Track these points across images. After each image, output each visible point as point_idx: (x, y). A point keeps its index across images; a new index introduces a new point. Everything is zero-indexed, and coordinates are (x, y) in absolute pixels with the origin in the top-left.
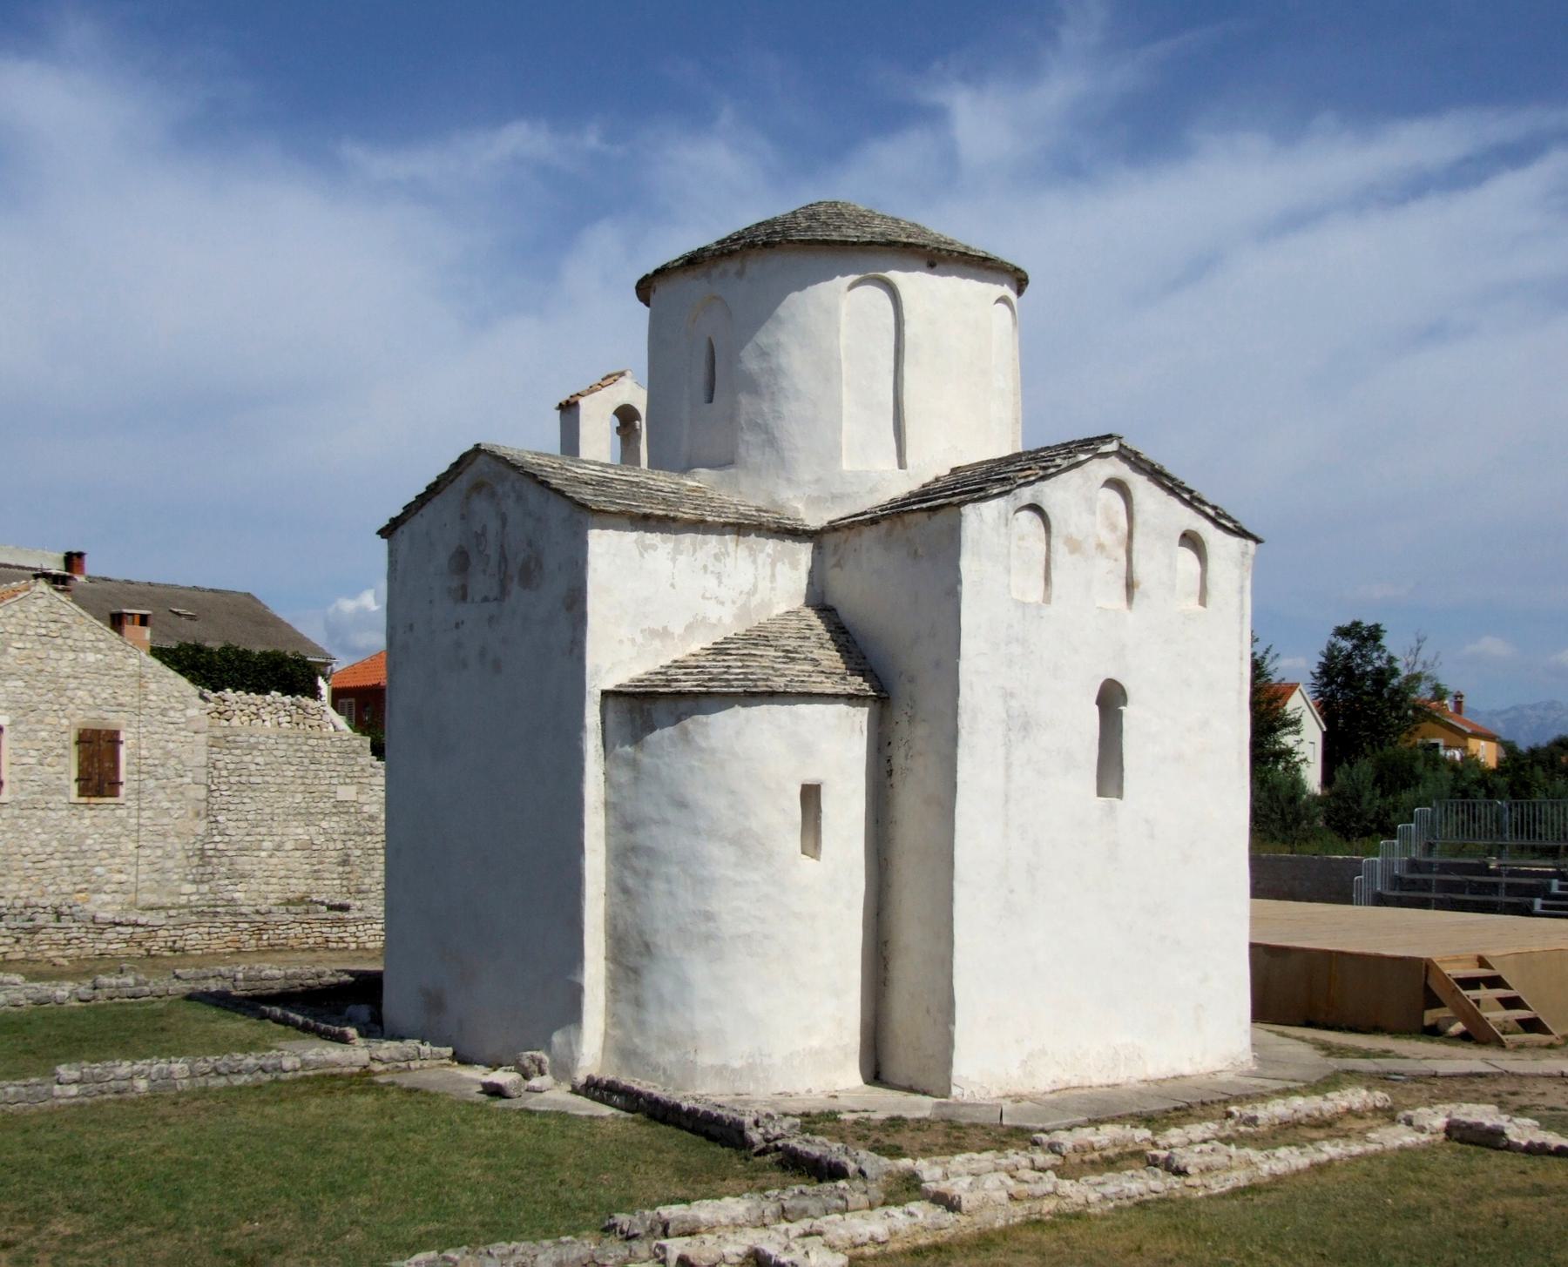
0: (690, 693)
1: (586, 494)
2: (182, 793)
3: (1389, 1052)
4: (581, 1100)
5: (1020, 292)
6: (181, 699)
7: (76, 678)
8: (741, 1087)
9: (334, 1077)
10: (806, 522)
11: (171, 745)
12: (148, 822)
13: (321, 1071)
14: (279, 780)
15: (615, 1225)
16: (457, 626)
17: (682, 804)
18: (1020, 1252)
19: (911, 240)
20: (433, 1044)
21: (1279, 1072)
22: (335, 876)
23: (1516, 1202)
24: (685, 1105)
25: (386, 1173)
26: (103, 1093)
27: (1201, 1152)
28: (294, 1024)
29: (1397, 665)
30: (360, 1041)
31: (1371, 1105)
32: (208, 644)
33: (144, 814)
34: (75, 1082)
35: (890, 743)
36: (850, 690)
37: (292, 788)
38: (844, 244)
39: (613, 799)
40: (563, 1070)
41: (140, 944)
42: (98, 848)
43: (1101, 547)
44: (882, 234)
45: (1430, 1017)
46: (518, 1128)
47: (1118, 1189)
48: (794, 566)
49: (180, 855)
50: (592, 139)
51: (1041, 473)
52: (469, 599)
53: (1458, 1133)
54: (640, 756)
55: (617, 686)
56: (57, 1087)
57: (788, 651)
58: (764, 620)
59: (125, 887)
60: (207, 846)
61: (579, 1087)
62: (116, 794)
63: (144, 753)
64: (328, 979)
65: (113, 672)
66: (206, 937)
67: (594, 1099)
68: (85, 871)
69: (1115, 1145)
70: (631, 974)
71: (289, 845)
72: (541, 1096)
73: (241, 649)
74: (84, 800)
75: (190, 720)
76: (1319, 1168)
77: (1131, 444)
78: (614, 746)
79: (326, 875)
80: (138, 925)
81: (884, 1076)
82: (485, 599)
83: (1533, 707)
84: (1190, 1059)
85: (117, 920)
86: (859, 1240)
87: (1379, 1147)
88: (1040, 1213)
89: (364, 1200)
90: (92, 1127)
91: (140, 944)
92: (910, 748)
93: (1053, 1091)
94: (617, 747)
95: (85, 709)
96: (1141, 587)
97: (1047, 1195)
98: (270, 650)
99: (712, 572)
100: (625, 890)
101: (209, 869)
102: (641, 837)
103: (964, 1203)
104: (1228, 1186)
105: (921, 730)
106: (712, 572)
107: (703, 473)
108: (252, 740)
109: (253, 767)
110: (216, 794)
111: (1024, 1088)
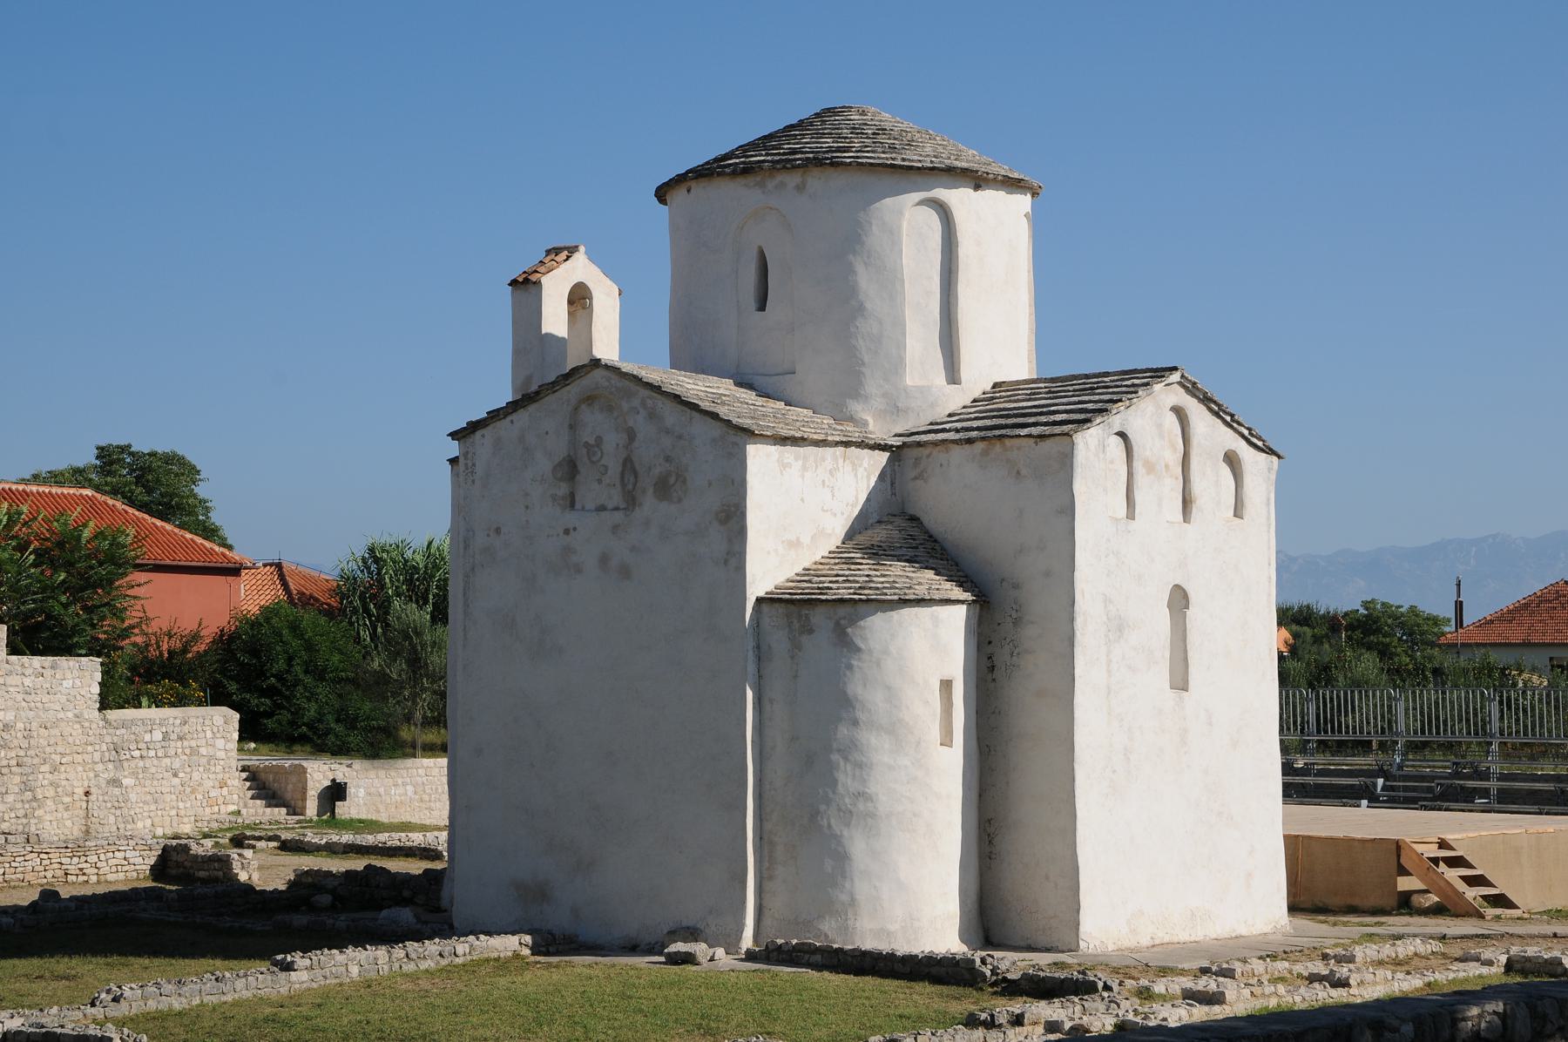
16: (567, 532)
52: (578, 506)
55: (767, 593)
84: (1245, 922)
96: (1197, 502)
99: (828, 486)
106: (828, 486)
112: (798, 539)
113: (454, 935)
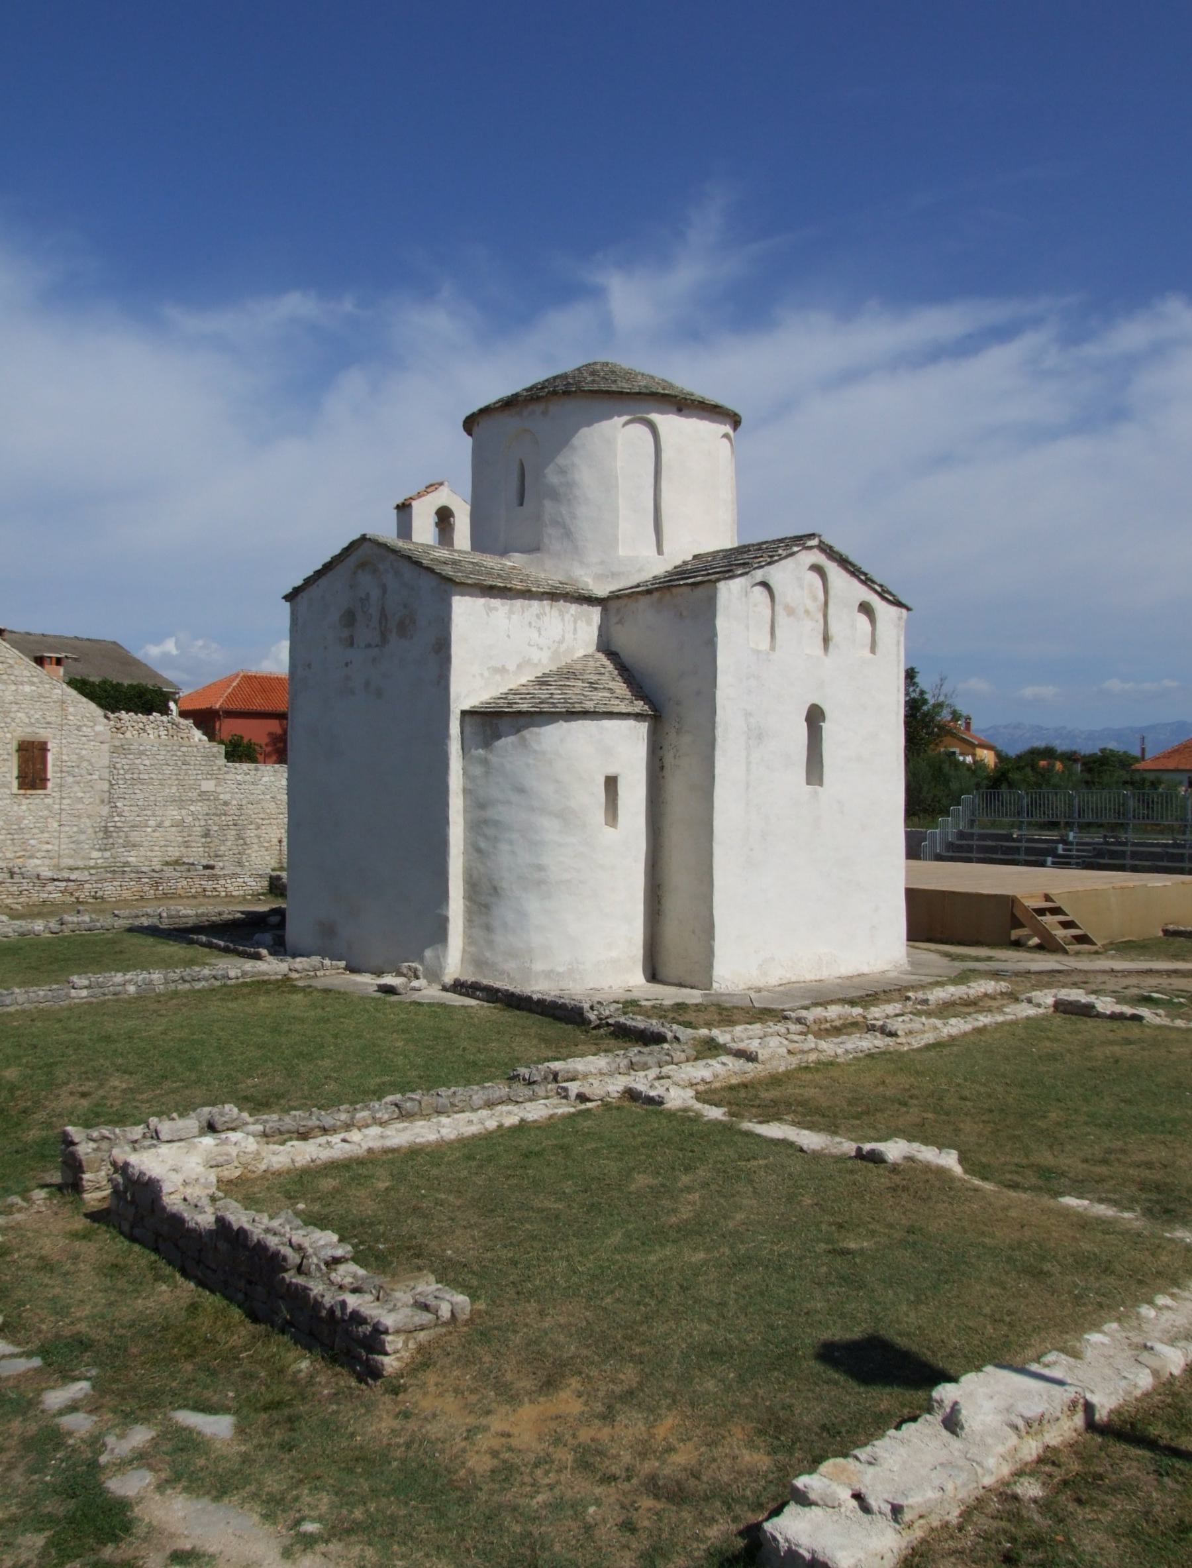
0: (528, 712)
1: (448, 571)
2: (92, 787)
3: (991, 957)
4: (450, 995)
5: (735, 429)
6: (91, 719)
7: (16, 703)
8: (563, 985)
9: (264, 982)
10: (595, 592)
11: (84, 752)
12: (67, 807)
13: (255, 979)
14: (160, 777)
15: (518, 1075)
16: (347, 665)
17: (521, 790)
18: (804, 1087)
19: (666, 392)
20: (331, 959)
21: (927, 971)
22: (200, 845)
23: (1117, 1048)
24: (535, 997)
25: (336, 1045)
26: (104, 994)
27: (903, 1021)
28: (218, 947)
29: (927, 696)
30: (270, 958)
31: (999, 991)
32: (91, 679)
33: (65, 801)
34: (86, 987)
35: (661, 748)
36: (637, 710)
37: (169, 782)
38: (621, 394)
39: (470, 786)
40: (434, 975)
41: (72, 894)
42: (32, 826)
43: (807, 612)
44: (645, 387)
45: (1015, 934)
46: (416, 1014)
47: (854, 1046)
48: (589, 623)
49: (90, 831)
50: (348, 305)
51: (769, 560)
52: (355, 646)
53: (1061, 1007)
54: (490, 756)
56: (73, 991)
57: (591, 683)
58: (569, 661)
59: (51, 854)
60: (109, 824)
61: (448, 987)
62: (44, 788)
63: (65, 758)
64: (226, 917)
65: (43, 700)
66: (119, 888)
67: (461, 994)
68: (24, 843)
69: (840, 1019)
70: (483, 909)
71: (167, 824)
72: (420, 993)
73: (114, 682)
74: (22, 792)
75: (97, 734)
76: (979, 1031)
77: (829, 540)
78: (470, 749)
79: (193, 844)
80: (70, 880)
81: (659, 977)
82: (369, 646)
83: (1006, 727)
85: (55, 877)
86: (694, 1081)
87: (1013, 1017)
88: (807, 1062)
89: (327, 1063)
90: (105, 1017)
91: (72, 894)
92: (677, 751)
93: (780, 985)
94: (473, 750)
95: (23, 726)
96: (834, 641)
97: (811, 1050)
98: (135, 683)
100: (479, 850)
101: (111, 841)
102: (491, 813)
103: (760, 1056)
104: (923, 1043)
105: (686, 739)
107: (517, 555)
108: (141, 748)
109: (142, 767)
110: (116, 787)
111: (761, 984)
112: (503, 666)
113: (285, 954)
